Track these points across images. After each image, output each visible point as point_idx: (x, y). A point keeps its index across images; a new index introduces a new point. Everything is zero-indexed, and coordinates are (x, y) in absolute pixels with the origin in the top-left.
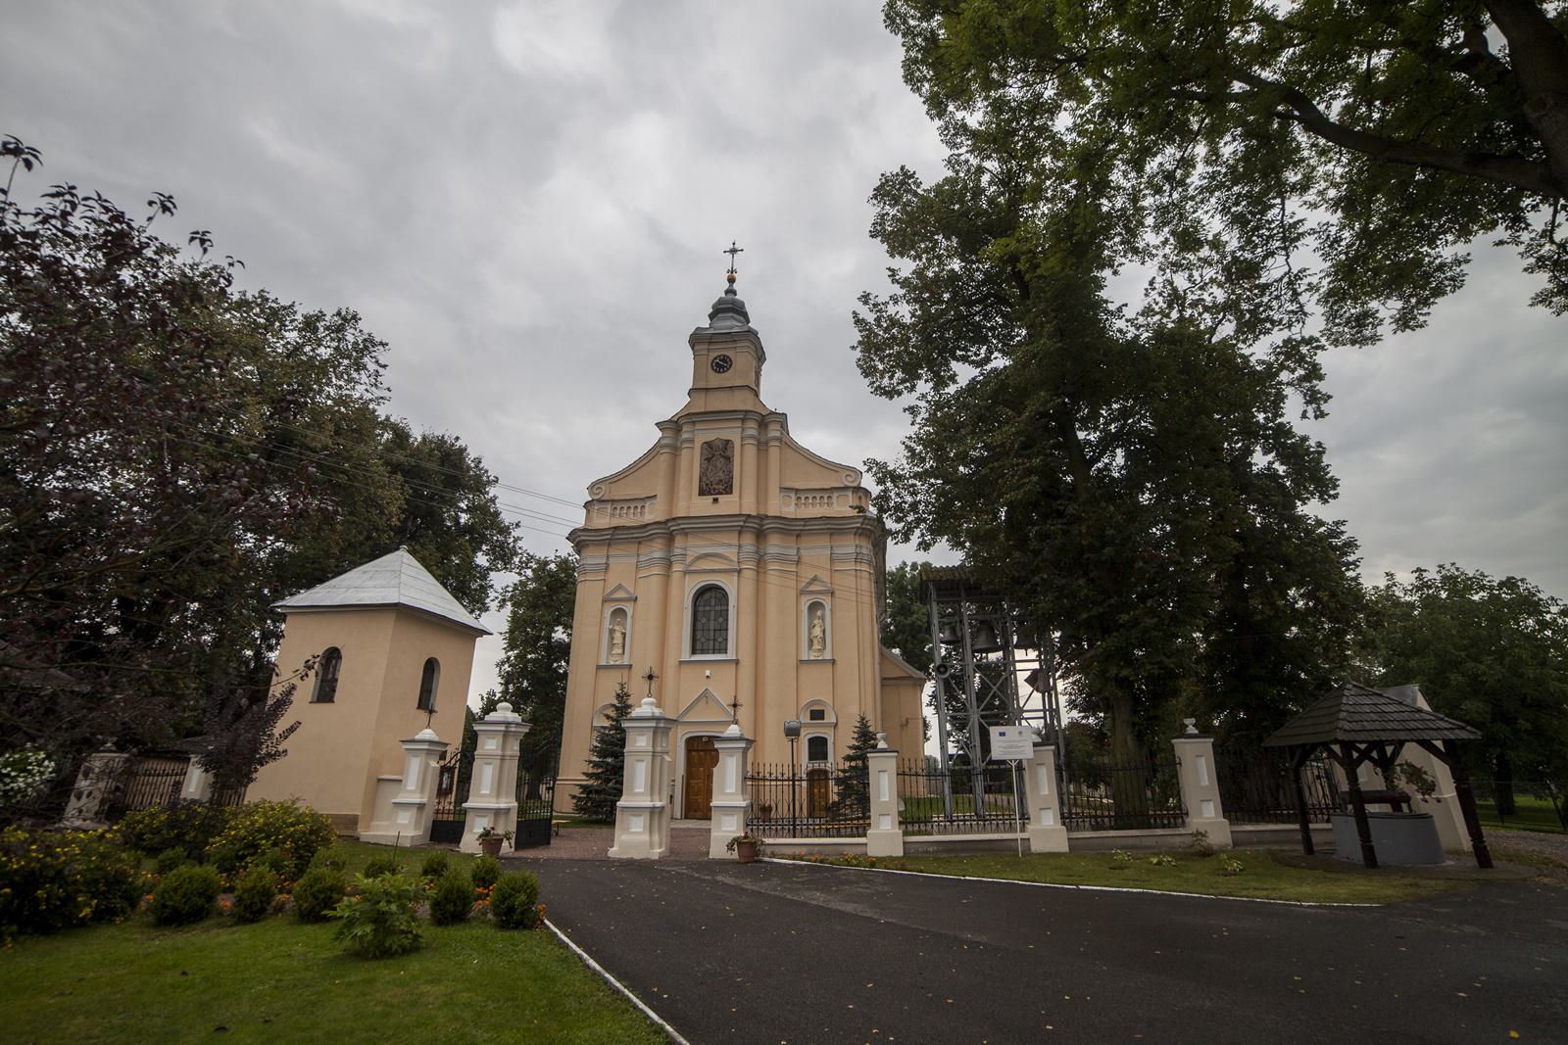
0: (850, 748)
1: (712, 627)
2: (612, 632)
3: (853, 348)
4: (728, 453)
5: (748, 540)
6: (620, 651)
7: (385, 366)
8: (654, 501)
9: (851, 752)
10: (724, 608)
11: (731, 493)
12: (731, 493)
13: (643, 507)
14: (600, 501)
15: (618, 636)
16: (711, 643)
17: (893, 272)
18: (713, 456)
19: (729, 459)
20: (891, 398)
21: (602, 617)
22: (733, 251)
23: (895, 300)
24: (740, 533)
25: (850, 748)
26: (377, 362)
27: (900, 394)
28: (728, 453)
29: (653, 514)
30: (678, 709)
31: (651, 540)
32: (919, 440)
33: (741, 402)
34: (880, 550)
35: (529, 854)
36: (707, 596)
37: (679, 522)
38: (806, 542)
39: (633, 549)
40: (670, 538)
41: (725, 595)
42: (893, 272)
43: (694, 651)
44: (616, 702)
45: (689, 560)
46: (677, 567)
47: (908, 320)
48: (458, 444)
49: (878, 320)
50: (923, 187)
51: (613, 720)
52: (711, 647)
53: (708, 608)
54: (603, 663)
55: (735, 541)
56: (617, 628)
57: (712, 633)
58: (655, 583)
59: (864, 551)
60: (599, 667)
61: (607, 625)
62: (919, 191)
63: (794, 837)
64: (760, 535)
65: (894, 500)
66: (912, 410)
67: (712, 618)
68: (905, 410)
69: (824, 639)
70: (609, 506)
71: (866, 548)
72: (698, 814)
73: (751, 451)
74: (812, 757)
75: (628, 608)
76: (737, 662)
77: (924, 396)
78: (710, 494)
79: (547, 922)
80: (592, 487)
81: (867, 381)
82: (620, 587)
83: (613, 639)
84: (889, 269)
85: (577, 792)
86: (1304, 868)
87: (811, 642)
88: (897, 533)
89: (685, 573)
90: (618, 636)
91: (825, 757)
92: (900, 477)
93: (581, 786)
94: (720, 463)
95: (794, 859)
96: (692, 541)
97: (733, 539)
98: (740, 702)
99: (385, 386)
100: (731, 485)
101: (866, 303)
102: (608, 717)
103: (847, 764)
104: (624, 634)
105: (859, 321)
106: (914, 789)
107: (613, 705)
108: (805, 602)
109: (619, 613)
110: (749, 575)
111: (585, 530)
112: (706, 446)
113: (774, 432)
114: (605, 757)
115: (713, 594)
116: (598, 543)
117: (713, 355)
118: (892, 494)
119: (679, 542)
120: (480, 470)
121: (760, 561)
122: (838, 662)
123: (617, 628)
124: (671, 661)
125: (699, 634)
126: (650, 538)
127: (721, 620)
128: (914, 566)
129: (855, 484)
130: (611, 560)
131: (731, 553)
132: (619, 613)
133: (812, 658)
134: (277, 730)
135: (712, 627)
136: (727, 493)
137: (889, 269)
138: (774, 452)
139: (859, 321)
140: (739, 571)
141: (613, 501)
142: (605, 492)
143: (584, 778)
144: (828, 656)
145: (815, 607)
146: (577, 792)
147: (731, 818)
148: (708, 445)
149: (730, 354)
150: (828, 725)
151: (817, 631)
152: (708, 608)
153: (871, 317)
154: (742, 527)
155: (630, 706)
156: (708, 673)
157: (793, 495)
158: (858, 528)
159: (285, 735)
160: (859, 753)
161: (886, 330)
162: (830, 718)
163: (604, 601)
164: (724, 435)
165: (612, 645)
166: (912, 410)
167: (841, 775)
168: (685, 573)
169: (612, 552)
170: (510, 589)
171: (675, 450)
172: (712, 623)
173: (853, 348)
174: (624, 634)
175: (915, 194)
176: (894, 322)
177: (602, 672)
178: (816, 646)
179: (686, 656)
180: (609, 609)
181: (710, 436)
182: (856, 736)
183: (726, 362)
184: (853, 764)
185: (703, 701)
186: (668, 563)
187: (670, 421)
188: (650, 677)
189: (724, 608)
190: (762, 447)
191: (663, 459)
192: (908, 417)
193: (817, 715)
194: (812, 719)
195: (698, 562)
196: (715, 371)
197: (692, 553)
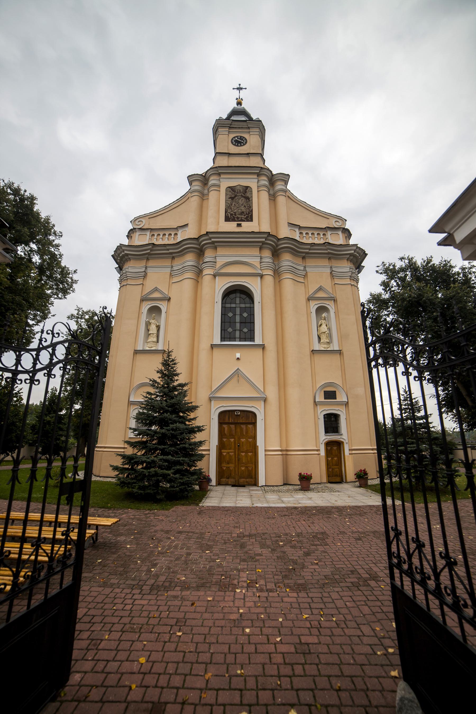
2: (148, 324)
4: (248, 195)
5: (267, 254)
6: (155, 339)
8: (186, 229)
11: (251, 220)
12: (251, 220)
13: (176, 234)
14: (141, 229)
15: (153, 329)
18: (236, 196)
19: (248, 199)
21: (140, 313)
22: (240, 89)
28: (248, 195)
29: (191, 233)
30: (211, 388)
31: (183, 255)
33: (254, 162)
36: (232, 296)
38: (310, 262)
39: (167, 262)
40: (200, 253)
45: (218, 265)
46: (208, 271)
48: (26, 194)
53: (233, 305)
54: (140, 348)
55: (258, 253)
56: (152, 321)
58: (188, 285)
60: (136, 352)
61: (144, 318)
64: (276, 254)
69: (330, 336)
70: (148, 233)
72: (231, 481)
73: (265, 195)
74: (327, 431)
75: (163, 306)
76: (263, 347)
78: (234, 220)
79: (86, 448)
80: (133, 222)
82: (156, 290)
83: (148, 330)
85: (119, 462)
86: (461, 499)
89: (215, 276)
90: (153, 329)
93: (124, 457)
94: (242, 201)
96: (221, 251)
97: (256, 251)
100: (252, 216)
104: (158, 327)
108: (314, 306)
109: (155, 310)
111: (129, 246)
112: (230, 189)
113: (279, 186)
114: (151, 425)
116: (139, 257)
117: (232, 136)
119: (209, 255)
121: (277, 273)
122: (344, 351)
123: (152, 321)
124: (204, 345)
126: (182, 253)
130: (149, 270)
131: (255, 261)
132: (155, 310)
136: (248, 221)
138: (281, 200)
140: (262, 276)
141: (151, 230)
142: (145, 224)
143: (126, 446)
144: (336, 347)
145: (321, 310)
146: (119, 462)
147: (381, 500)
148: (231, 189)
149: (246, 136)
150: (340, 403)
151: (324, 328)
152: (233, 305)
156: (238, 355)
157: (297, 230)
158: (351, 255)
162: (341, 397)
163: (142, 300)
164: (244, 183)
165: (148, 334)
168: (215, 276)
169: (151, 263)
171: (203, 196)
174: (158, 327)
177: (139, 357)
178: (324, 339)
179: (217, 340)
180: (146, 306)
181: (233, 183)
183: (242, 140)
185: (235, 378)
186: (199, 272)
187: (201, 175)
189: (252, 306)
190: (273, 197)
191: (195, 201)
193: (330, 395)
194: (325, 399)
195: (227, 267)
196: (235, 145)
197: (221, 261)
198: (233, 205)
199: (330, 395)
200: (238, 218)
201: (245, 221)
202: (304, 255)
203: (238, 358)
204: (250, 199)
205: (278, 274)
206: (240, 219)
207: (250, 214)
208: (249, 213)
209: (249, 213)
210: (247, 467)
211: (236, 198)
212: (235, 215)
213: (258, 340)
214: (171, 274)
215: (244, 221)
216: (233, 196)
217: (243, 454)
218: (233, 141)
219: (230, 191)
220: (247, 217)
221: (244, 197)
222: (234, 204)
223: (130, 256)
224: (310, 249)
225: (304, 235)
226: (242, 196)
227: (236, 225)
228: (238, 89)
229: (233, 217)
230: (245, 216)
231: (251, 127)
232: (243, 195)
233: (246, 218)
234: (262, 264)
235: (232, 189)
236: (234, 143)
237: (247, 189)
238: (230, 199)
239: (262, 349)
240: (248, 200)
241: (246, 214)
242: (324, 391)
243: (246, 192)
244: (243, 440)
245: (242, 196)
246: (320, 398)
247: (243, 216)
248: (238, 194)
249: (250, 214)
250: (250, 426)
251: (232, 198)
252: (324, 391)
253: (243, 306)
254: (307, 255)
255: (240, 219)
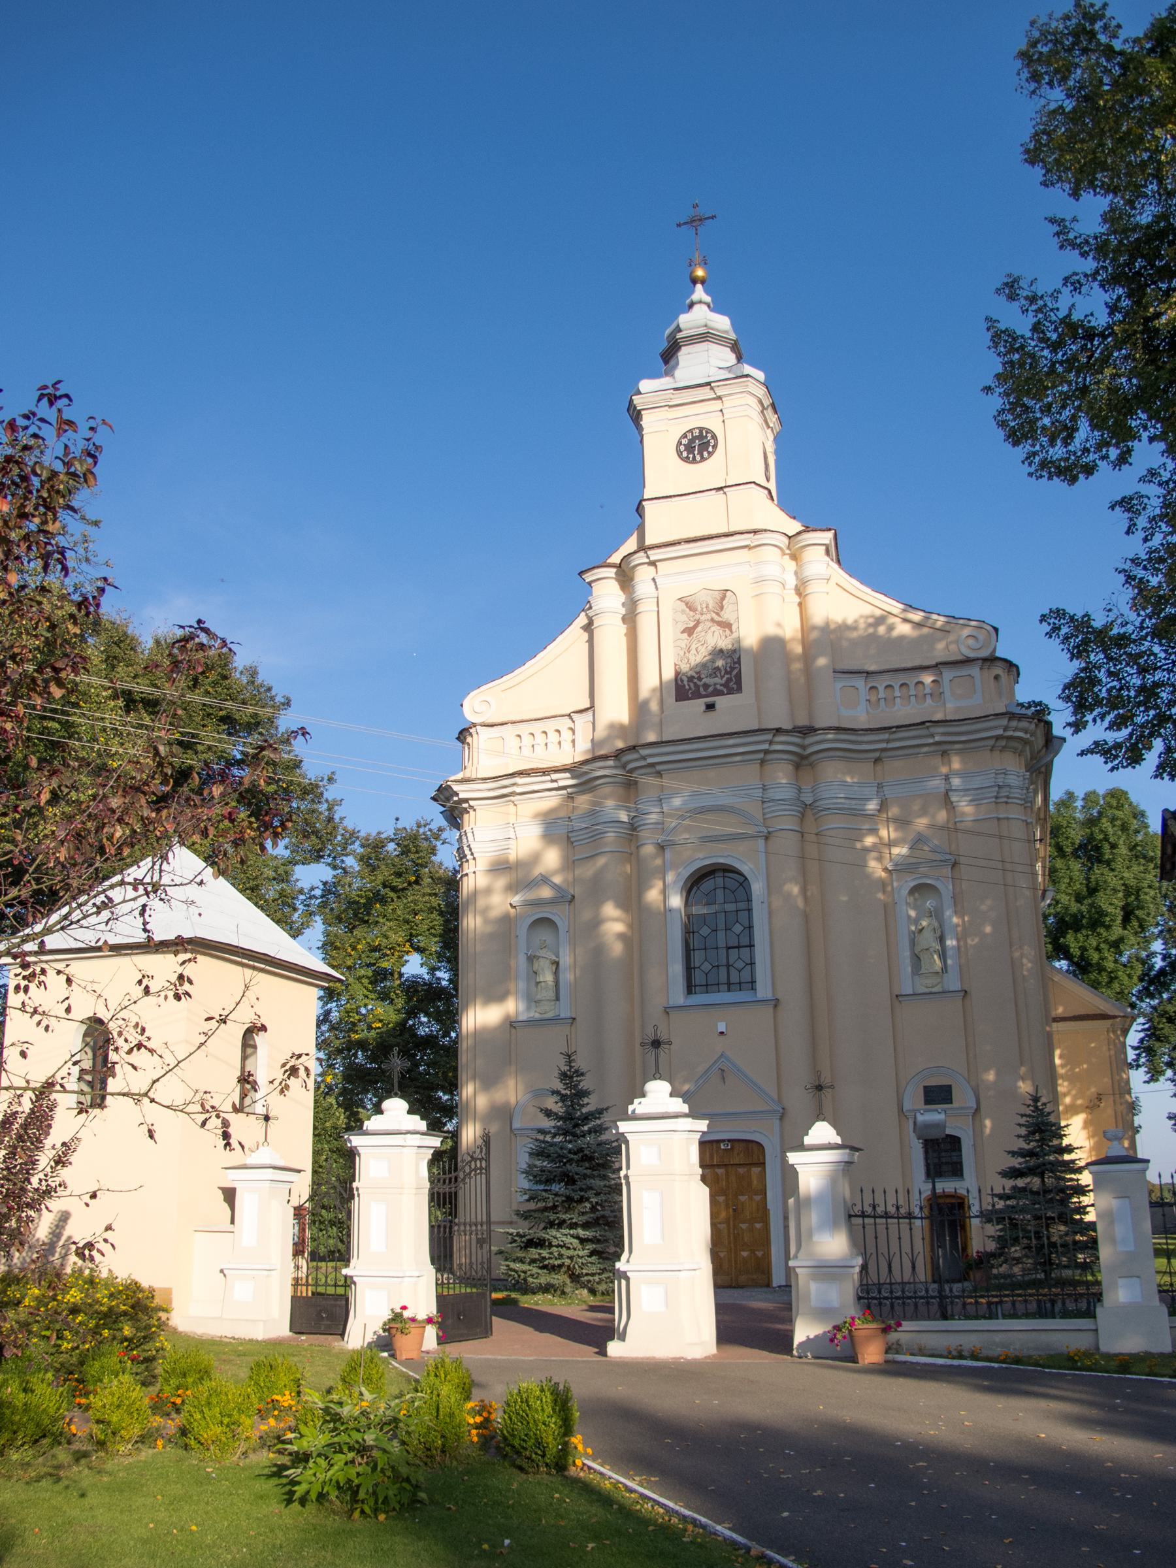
0: (1013, 1154)
1: (722, 944)
3: (988, 389)
4: (727, 615)
5: (781, 776)
7: (96, 523)
9: (1017, 1162)
10: (742, 906)
11: (739, 689)
12: (739, 689)
16: (723, 970)
17: (1061, 226)
18: (698, 623)
20: (1073, 480)
23: (1074, 283)
24: (763, 762)
25: (1013, 1154)
26: (83, 518)
27: (1089, 470)
28: (727, 615)
32: (1154, 561)
34: (1041, 773)
35: (455, 1350)
36: (708, 885)
37: (644, 752)
41: (743, 883)
42: (1061, 226)
43: (690, 989)
44: (559, 1086)
47: (1101, 319)
49: (1036, 328)
50: (1123, 34)
51: (559, 1118)
52: (723, 977)
57: (723, 952)
59: (1013, 780)
62: (1117, 45)
63: (945, 1317)
65: (1106, 685)
66: (1127, 504)
67: (721, 925)
68: (1112, 508)
71: (1014, 770)
77: (1152, 473)
78: (697, 695)
81: (1021, 451)
84: (1052, 221)
87: (916, 959)
88: (1118, 746)
91: (957, 1171)
92: (1122, 640)
95: (961, 1356)
98: (826, 1079)
99: (101, 559)
100: (739, 676)
101: (1012, 297)
102: (548, 1113)
103: (1009, 1183)
105: (1002, 338)
106: (473, 1216)
107: (557, 1093)
110: (787, 843)
115: (720, 881)
118: (1102, 675)
120: (258, 688)
125: (698, 957)
127: (738, 928)
128: (1090, 797)
129: (985, 653)
133: (923, 990)
134: (44, 1160)
135: (722, 944)
136: (731, 692)
137: (1052, 221)
139: (1002, 338)
153: (1022, 325)
154: (766, 752)
155: (584, 1094)
156: (722, 1027)
158: (998, 738)
159: (60, 1161)
160: (1033, 1162)
161: (1055, 347)
162: (963, 1097)
166: (1127, 504)
167: (1000, 1204)
170: (318, 892)
172: (721, 935)
173: (988, 389)
175: (1109, 52)
176: (1070, 327)
179: (678, 996)
182: (1023, 1131)
184: (1020, 1183)
188: (656, 1044)
192: (1121, 518)
198: (693, 651)
199: (938, 1095)
200: (706, 686)
201: (723, 694)
202: (877, 754)
203: (722, 1033)
204: (734, 628)
205: (814, 814)
206: (711, 689)
207: (735, 672)
208: (732, 669)
209: (732, 669)
210: (753, 1252)
211: (699, 629)
212: (700, 679)
213: (763, 990)
214: (568, 838)
215: (720, 693)
216: (691, 624)
217: (744, 1226)
218: (682, 448)
219: (683, 612)
220: (729, 680)
221: (720, 624)
222: (694, 647)
223: (471, 803)
224: (888, 741)
225: (882, 694)
226: (712, 620)
227: (704, 708)
228: (690, 222)
229: (695, 684)
230: (722, 677)
231: (726, 396)
232: (716, 618)
233: (726, 685)
234: (766, 805)
235: (687, 604)
236: (685, 454)
237: (723, 598)
238: (685, 635)
239: (771, 1010)
240: (728, 632)
241: (726, 672)
242: (925, 1087)
243: (722, 608)
244: (742, 1198)
245: (712, 620)
246: (913, 1099)
247: (717, 680)
248: (703, 618)
249: (735, 672)
250: (756, 1170)
251: (689, 631)
252: (925, 1087)
253: (730, 907)
254: (884, 754)
255: (711, 689)
